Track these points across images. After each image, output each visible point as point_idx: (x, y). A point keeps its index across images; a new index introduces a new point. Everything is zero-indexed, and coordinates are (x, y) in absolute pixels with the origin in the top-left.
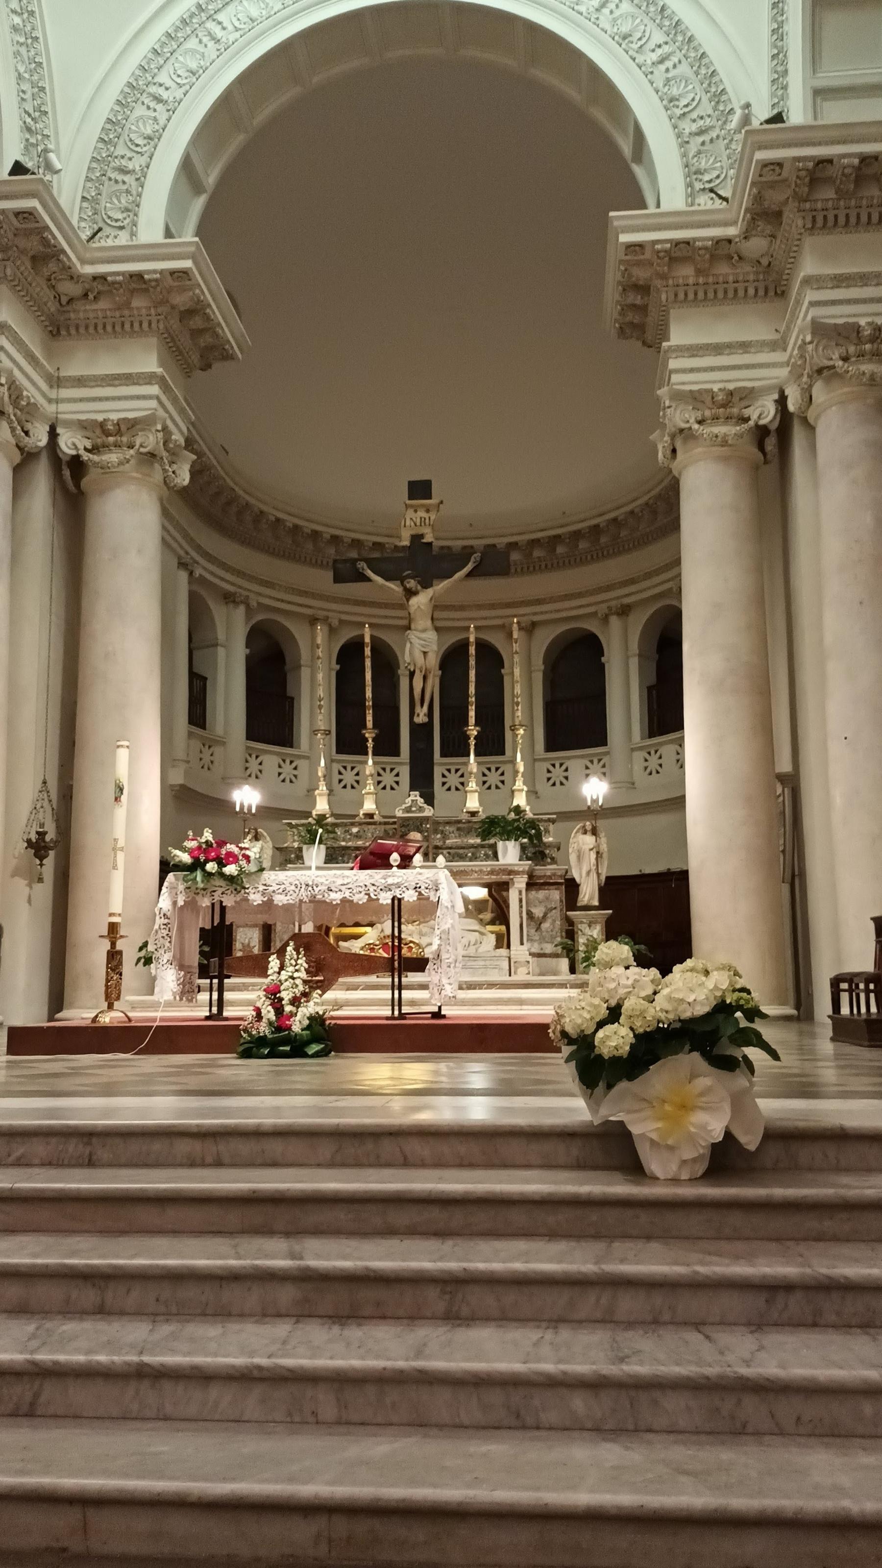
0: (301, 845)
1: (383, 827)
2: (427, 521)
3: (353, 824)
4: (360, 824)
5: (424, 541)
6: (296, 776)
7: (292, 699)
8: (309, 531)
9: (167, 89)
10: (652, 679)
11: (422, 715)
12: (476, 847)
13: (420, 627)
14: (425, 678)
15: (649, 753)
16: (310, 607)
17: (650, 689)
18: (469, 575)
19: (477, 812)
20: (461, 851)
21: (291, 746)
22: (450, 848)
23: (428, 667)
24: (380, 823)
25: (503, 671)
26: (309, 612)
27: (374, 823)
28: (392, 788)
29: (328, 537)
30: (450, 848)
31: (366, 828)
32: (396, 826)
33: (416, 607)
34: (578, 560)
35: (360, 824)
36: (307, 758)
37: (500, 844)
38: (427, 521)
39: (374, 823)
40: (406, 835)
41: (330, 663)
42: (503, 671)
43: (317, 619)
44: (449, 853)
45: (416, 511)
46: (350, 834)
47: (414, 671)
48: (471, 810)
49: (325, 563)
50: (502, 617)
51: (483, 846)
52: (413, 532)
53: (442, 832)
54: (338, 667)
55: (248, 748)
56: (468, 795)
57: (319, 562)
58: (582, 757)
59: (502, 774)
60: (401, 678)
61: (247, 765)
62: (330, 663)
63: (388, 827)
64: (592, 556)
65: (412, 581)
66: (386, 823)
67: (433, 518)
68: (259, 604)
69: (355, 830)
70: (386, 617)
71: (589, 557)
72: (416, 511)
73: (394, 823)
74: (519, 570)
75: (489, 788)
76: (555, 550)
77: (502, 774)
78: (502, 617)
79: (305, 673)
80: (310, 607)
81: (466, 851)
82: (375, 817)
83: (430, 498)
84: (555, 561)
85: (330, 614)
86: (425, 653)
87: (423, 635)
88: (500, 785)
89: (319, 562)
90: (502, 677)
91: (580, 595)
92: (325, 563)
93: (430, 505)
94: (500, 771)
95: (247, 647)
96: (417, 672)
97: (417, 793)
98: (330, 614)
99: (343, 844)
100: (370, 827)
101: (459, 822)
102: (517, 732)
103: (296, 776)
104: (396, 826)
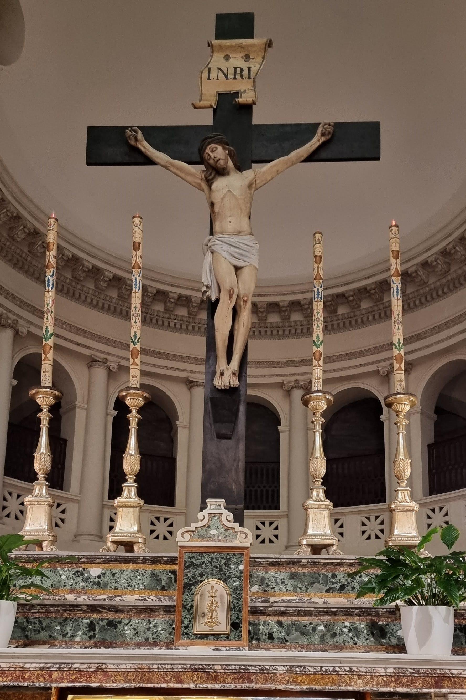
0: (333, 572)
1: (149, 568)
2: (246, 72)
3: (91, 560)
4: (107, 561)
5: (240, 100)
6: (62, 520)
7: (65, 441)
8: (90, 267)
9: (219, 69)
10: (432, 440)
11: (228, 374)
12: (334, 613)
13: (230, 227)
14: (235, 312)
15: (433, 510)
16: (89, 348)
17: (429, 446)
18: (310, 158)
19: (326, 546)
20: (304, 620)
21: (61, 489)
22: (283, 613)
23: (242, 292)
24: (145, 561)
25: (279, 428)
26: (87, 352)
27: (134, 561)
28: (165, 538)
29: (111, 276)
30: (283, 613)
31: (116, 568)
32: (175, 567)
33: (225, 191)
34: (359, 321)
35: (107, 561)
36: (78, 501)
37: (405, 610)
38: (246, 72)
39: (134, 561)
40: (196, 583)
41: (107, 408)
42: (279, 428)
43: (96, 361)
44: (280, 624)
45: (227, 58)
46: (86, 580)
47: (218, 301)
48: (314, 542)
49: (106, 306)
50: (280, 376)
51: (348, 612)
52: (222, 89)
53: (262, 581)
54: (115, 413)
55: (4, 484)
56: (310, 512)
57: (100, 304)
58: (359, 513)
59: (277, 528)
60: (179, 430)
61: (5, 504)
62: (107, 408)
63: (159, 568)
64: (374, 317)
65: (220, 149)
66: (155, 561)
67: (254, 70)
68: (28, 332)
69: (95, 571)
70: (167, 368)
71: (371, 318)
72: (227, 58)
73: (172, 561)
74: (299, 331)
75: (263, 542)
76: (335, 311)
77: (277, 528)
78: (280, 376)
79: (80, 415)
80: (89, 348)
81: (314, 620)
82: (136, 548)
83: (251, 36)
84: (335, 323)
85: (109, 358)
86: (237, 269)
87: (234, 240)
88: (274, 539)
89: (100, 304)
90: (278, 434)
91: (361, 354)
92: (106, 306)
93: (253, 45)
94: (274, 526)
95: (14, 377)
96: (224, 297)
97: (222, 501)
98: (109, 358)
99: (70, 598)
100: (124, 566)
101: (294, 562)
102: (399, 408)
103: (62, 520)
104: (175, 567)
